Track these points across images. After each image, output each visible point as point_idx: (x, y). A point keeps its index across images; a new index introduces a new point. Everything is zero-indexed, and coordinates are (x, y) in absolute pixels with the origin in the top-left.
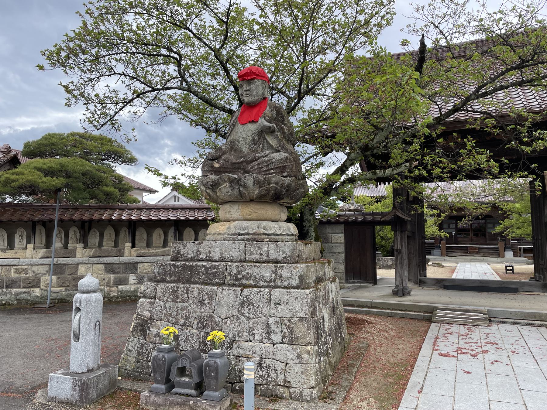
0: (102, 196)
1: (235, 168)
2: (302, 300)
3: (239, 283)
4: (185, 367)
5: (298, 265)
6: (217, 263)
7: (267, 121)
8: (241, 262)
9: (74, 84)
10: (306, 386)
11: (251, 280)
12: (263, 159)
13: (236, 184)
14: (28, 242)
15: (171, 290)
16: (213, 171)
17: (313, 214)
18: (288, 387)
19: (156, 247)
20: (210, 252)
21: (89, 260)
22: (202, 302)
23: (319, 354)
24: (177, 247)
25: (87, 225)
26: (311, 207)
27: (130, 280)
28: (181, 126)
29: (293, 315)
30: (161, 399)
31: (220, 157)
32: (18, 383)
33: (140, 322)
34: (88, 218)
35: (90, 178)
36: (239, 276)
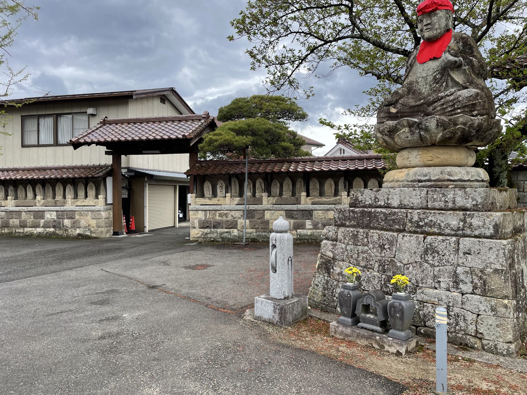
0: (282, 152)
1: (414, 111)
2: (498, 250)
3: (421, 230)
4: (369, 305)
5: (492, 213)
6: (397, 210)
7: (452, 55)
8: (423, 209)
9: (258, 48)
10: (502, 340)
11: (434, 228)
12: (448, 98)
13: (416, 128)
14: (227, 192)
15: (351, 234)
16: (389, 117)
17: (505, 158)
18: (480, 339)
19: (328, 196)
20: (388, 199)
21: (272, 207)
22: (382, 247)
23: (517, 309)
24: (355, 194)
25: (269, 176)
26: (503, 150)
27: (307, 225)
28: (347, 77)
29: (487, 266)
30: (348, 331)
31: (397, 101)
32: (231, 303)
33: (324, 261)
34: (271, 171)
35: (271, 135)
36: (421, 223)
